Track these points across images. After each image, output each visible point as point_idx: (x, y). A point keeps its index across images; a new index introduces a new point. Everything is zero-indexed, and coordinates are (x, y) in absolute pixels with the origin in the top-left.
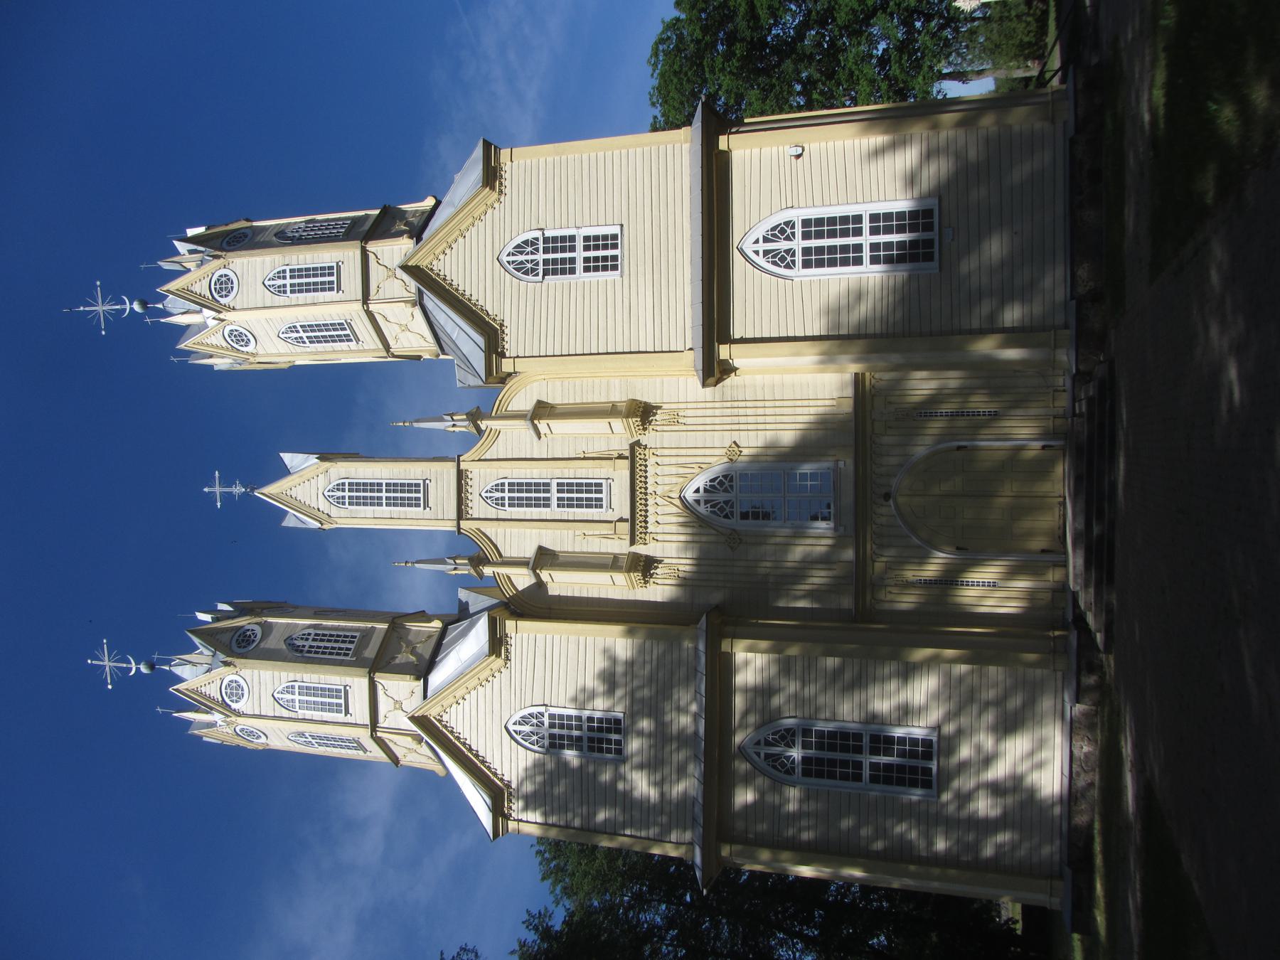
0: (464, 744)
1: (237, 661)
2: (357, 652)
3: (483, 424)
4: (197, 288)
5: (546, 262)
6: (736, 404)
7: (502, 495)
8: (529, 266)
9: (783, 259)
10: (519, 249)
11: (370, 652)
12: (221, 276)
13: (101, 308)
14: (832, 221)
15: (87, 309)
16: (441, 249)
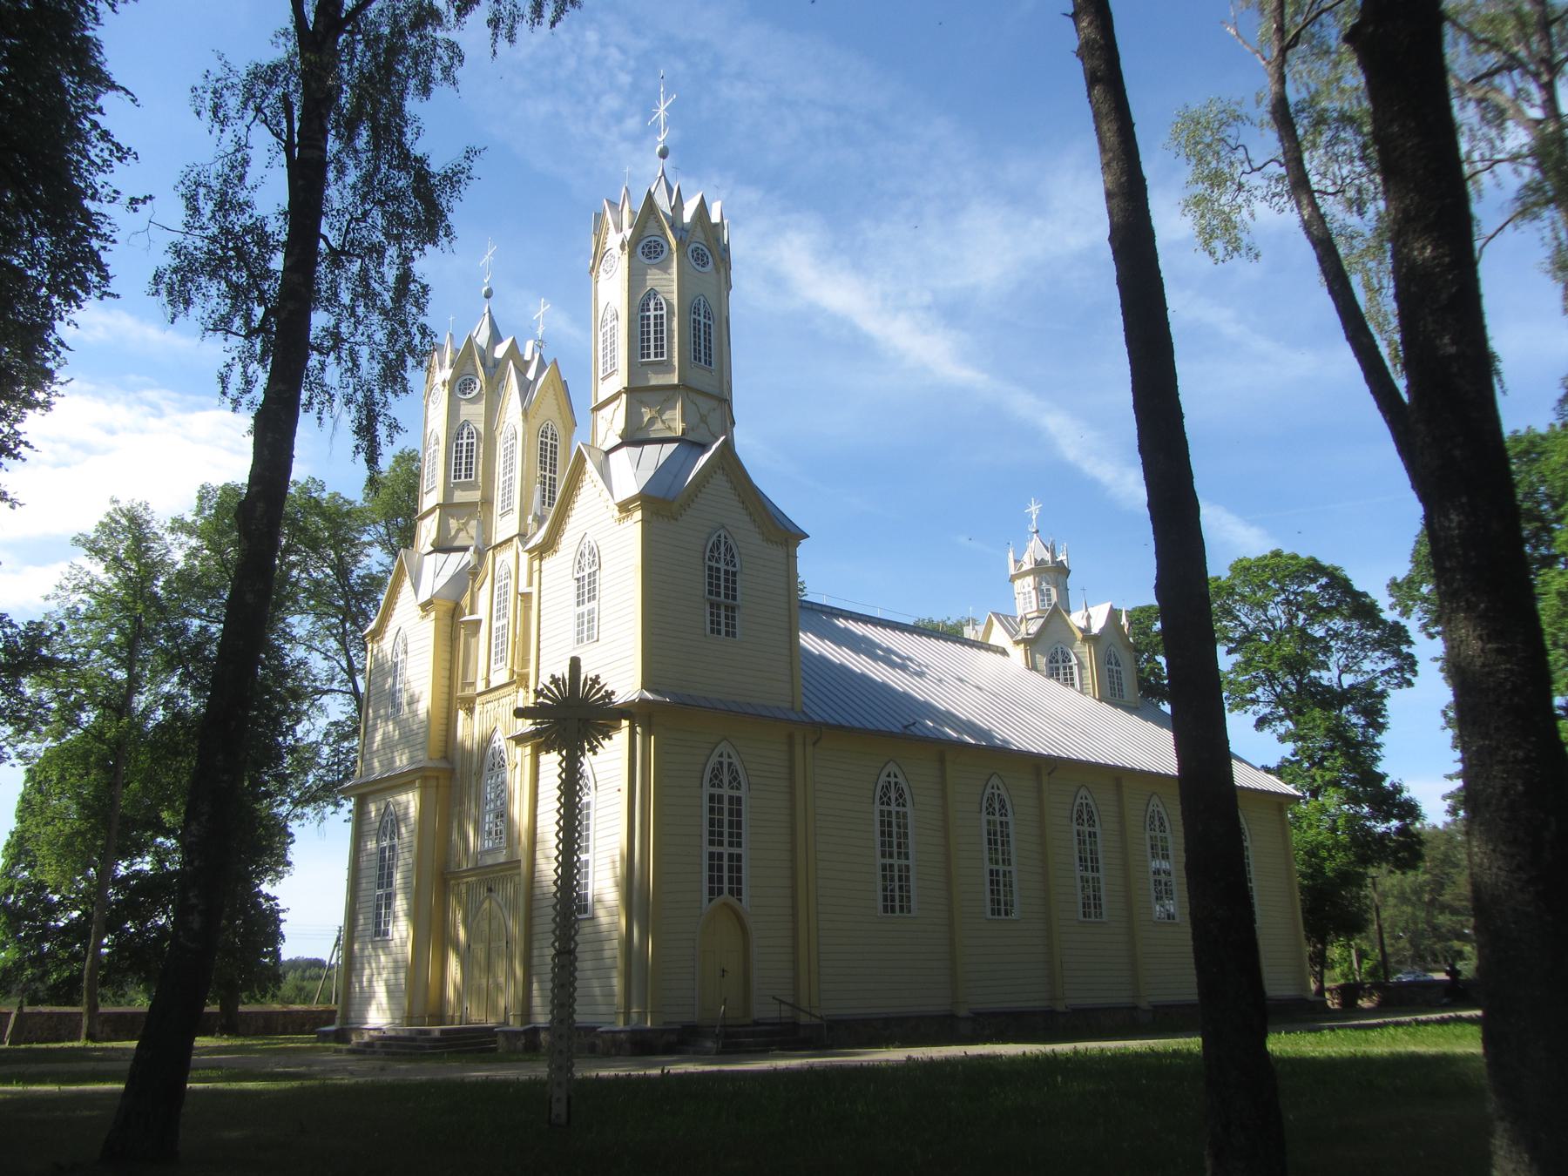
7: (1060, 661)
9: (716, 777)
10: (729, 549)
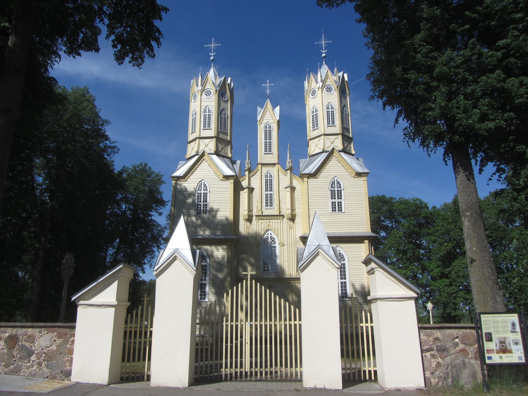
0: (197, 167)
1: (217, 94)
2: (221, 132)
3: (289, 171)
4: (328, 80)
5: (335, 191)
6: (295, 245)
8: (334, 186)
11: (221, 136)
12: (332, 88)
13: (323, 42)
14: (345, 271)
15: (323, 38)
16: (339, 160)
